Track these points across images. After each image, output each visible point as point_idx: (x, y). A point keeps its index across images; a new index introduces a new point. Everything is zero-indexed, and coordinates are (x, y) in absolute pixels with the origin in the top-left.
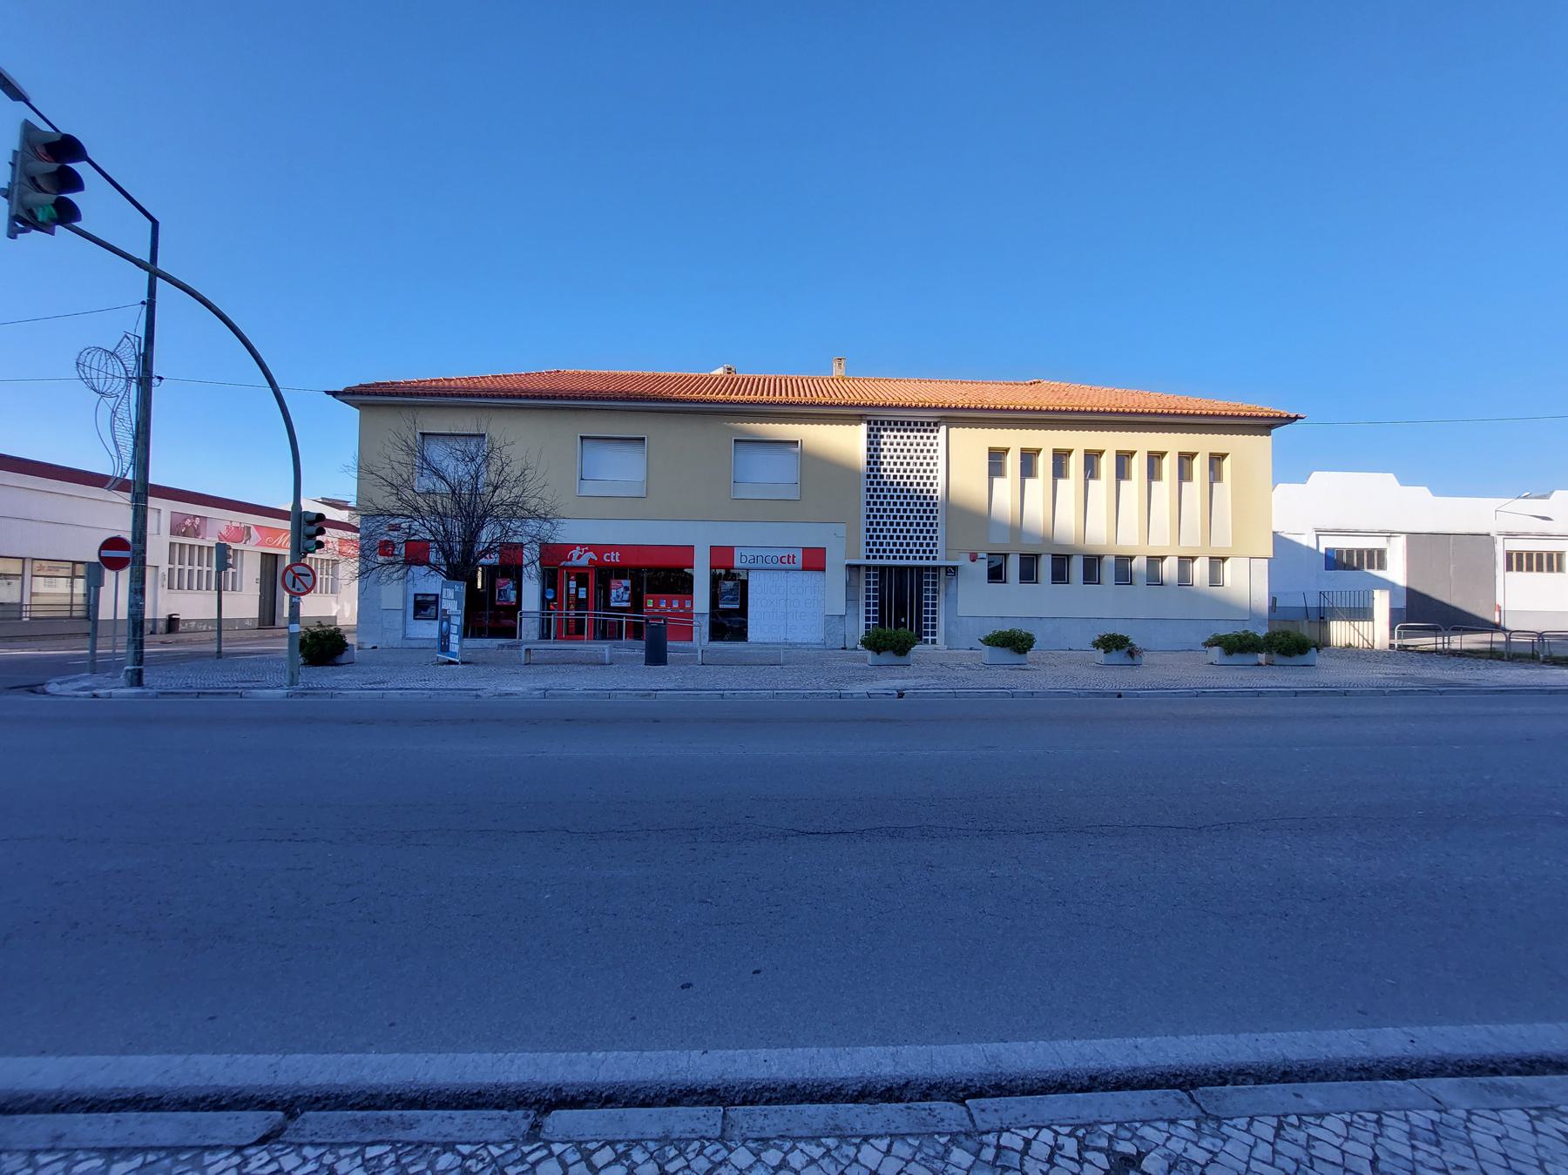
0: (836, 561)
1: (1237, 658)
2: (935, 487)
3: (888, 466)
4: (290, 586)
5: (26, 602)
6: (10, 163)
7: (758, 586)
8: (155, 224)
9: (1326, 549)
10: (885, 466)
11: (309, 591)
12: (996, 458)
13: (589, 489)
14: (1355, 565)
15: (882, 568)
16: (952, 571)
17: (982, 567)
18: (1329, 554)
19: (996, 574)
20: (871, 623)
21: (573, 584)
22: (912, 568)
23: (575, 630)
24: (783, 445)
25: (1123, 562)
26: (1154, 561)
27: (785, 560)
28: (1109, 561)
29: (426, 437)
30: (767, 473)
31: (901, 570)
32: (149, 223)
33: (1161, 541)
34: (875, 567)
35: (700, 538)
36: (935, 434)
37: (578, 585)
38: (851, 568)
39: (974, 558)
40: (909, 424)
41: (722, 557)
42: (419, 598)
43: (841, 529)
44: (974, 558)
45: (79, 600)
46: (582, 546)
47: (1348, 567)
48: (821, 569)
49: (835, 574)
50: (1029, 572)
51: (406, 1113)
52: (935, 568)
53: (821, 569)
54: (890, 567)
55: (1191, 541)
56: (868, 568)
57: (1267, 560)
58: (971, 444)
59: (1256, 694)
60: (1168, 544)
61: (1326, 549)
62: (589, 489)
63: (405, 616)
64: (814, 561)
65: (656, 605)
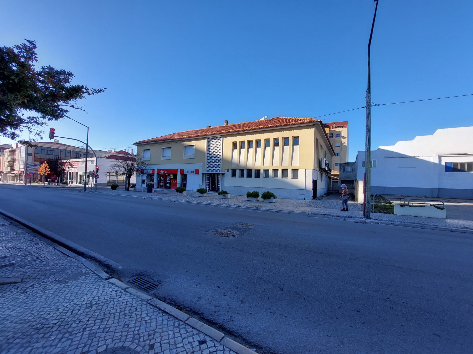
0: (201, 172)
1: (250, 199)
2: (220, 153)
3: (212, 149)
4: (95, 177)
5: (117, 180)
6: (11, 145)
7: (188, 177)
8: (88, 128)
9: (446, 163)
10: (211, 149)
11: (98, 178)
12: (235, 145)
13: (164, 158)
14: (466, 170)
15: (210, 174)
16: (223, 174)
17: (230, 173)
18: (448, 165)
19: (234, 175)
20: (208, 187)
21: (162, 177)
22: (216, 173)
23: (162, 187)
24: (188, 146)
25: (266, 171)
26: (275, 171)
27: (192, 172)
28: (262, 171)
29: (186, 147)
30: (190, 153)
31: (214, 174)
32: (87, 128)
33: (267, 165)
34: (209, 173)
35: (178, 167)
36: (220, 140)
37: (162, 178)
38: (203, 174)
39: (228, 171)
40: (216, 138)
41: (182, 171)
42: (143, 180)
43: (202, 165)
44: (228, 171)
45: (125, 180)
46: (162, 170)
47: (462, 170)
48: (198, 174)
49: (200, 175)
50: (250, 175)
51: (98, 255)
52: (219, 174)
53: (198, 174)
54: (212, 173)
55: (276, 165)
56: (207, 173)
57: (312, 170)
58: (229, 141)
59: (197, 204)
60: (278, 166)
61: (446, 163)
62: (164, 158)
63: (141, 183)
64: (197, 172)
65: (173, 181)
